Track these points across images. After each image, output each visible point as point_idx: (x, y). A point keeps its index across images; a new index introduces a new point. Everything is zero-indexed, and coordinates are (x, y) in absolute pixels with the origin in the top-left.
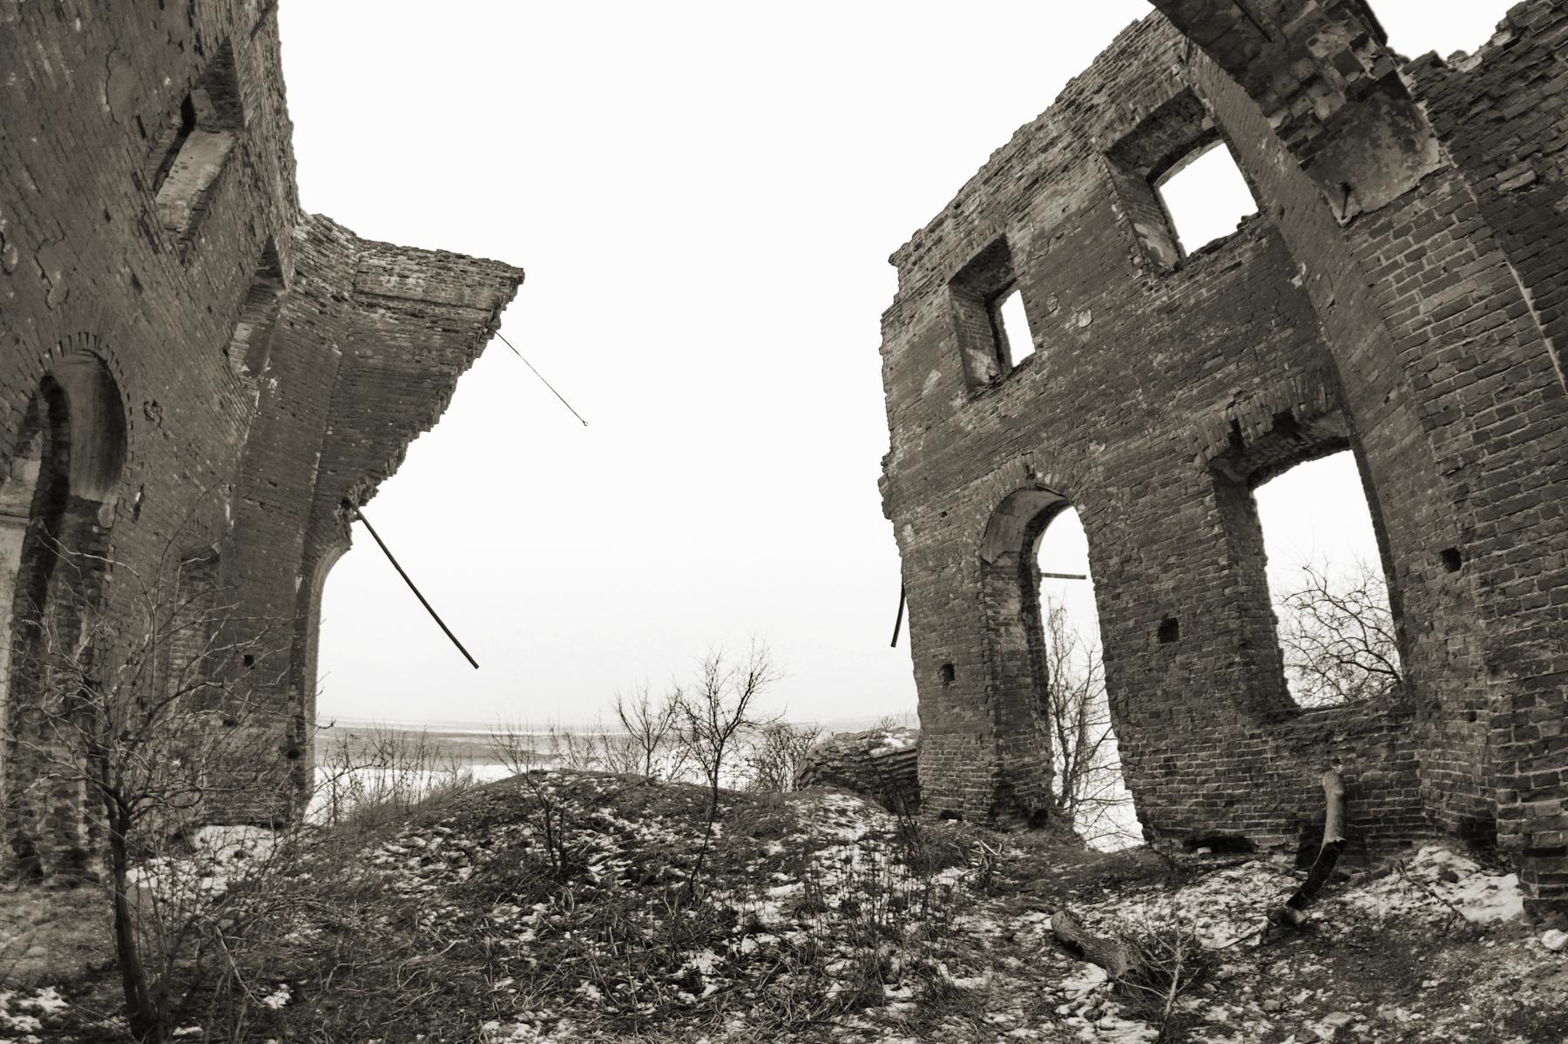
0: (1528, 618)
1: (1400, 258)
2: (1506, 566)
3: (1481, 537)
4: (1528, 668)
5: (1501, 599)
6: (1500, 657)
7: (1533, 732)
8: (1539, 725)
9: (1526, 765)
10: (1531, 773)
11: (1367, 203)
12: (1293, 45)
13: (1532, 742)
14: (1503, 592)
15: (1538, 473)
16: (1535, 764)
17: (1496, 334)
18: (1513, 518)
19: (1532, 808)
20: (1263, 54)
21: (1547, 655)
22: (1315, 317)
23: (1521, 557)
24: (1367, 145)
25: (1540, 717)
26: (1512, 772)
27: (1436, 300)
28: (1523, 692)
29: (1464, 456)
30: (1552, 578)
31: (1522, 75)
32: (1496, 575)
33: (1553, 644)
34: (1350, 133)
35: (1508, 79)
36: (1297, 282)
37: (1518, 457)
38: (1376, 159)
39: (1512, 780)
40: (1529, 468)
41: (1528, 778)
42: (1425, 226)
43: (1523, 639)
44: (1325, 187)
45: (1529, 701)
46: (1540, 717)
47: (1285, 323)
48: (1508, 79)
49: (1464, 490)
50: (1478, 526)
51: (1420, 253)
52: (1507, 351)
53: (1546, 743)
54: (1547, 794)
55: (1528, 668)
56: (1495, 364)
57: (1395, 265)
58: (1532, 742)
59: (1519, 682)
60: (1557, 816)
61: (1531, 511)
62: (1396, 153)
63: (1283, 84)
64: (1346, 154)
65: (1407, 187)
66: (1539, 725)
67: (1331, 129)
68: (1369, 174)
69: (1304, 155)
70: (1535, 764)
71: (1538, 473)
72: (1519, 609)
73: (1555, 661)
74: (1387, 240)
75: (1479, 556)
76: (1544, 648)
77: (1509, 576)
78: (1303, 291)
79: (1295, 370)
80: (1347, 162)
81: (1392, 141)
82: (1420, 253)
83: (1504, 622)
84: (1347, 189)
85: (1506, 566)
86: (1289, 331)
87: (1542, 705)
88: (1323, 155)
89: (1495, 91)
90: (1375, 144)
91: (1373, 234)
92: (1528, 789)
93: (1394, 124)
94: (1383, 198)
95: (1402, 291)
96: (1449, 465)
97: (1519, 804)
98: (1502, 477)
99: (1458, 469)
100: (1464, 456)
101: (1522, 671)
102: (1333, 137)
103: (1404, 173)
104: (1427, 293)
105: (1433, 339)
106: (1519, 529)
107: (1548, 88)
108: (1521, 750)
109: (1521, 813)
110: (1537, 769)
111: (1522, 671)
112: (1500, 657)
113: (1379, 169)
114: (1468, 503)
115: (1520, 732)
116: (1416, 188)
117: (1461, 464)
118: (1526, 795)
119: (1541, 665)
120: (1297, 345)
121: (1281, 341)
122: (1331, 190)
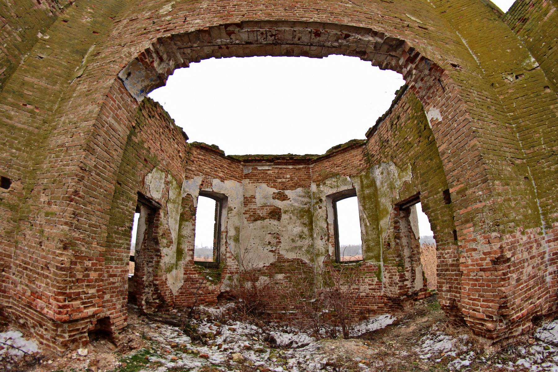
0: (82, 233)
1: (117, 102)
2: (82, 212)
3: (79, 197)
4: (78, 252)
5: (77, 223)
6: (70, 244)
7: (74, 276)
8: (77, 273)
9: (71, 288)
10: (72, 291)
11: (126, 82)
12: (173, 54)
13: (74, 279)
14: (78, 221)
15: (102, 190)
16: (73, 288)
17: (116, 147)
18: (91, 198)
19: (72, 305)
20: (175, 47)
21: (83, 249)
22: (29, 50)
23: (87, 212)
24: (143, 79)
25: (78, 271)
26: (66, 290)
27: (113, 121)
28: (74, 260)
29: (90, 168)
30: (93, 224)
31: (149, 111)
32: (79, 214)
33: (86, 246)
34: (147, 74)
35: (148, 108)
36: (40, 35)
37: (100, 182)
38: (138, 82)
39: (65, 293)
40: (101, 187)
41: (71, 293)
42: (126, 105)
43: (78, 240)
44: (129, 66)
45: (75, 264)
46: (78, 271)
47: (22, 36)
48: (148, 108)
49: (83, 178)
50: (81, 193)
51: (120, 108)
52: (114, 153)
53: (78, 280)
54: (76, 299)
55: (78, 252)
56: (111, 153)
57: (115, 101)
58: (74, 279)
59: (75, 256)
60: (79, 308)
61: (96, 200)
62: (140, 88)
63: (161, 49)
64: (140, 72)
65: (132, 94)
66: (77, 273)
67: (149, 67)
68: (134, 81)
69: (141, 58)
70: (73, 288)
71: (102, 190)
72: (80, 229)
73: (86, 252)
74: (119, 94)
75: (77, 203)
76: (84, 246)
77: (82, 217)
78: (37, 40)
79: (5, 50)
80: (137, 73)
81: (143, 86)
82: (120, 108)
83: (75, 231)
84: (129, 74)
85: (82, 212)
86: (20, 40)
87: (79, 267)
88: (140, 65)
89: (146, 105)
90: (143, 81)
91: (119, 89)
92: (71, 297)
93: (148, 85)
94: (128, 87)
95: (111, 109)
96: (84, 166)
97: (67, 303)
98: (94, 184)
99: (85, 170)
100: (90, 168)
101: (76, 252)
102: (146, 68)
103: (135, 92)
104: (113, 118)
105: (105, 129)
106: (90, 203)
107: (149, 119)
108: (70, 281)
109: (67, 306)
110: (74, 289)
111: (76, 252)
112: (70, 244)
113: (135, 84)
114: (81, 183)
115: (71, 274)
116: (132, 97)
117: (87, 169)
118: (70, 299)
119: (82, 252)
120: (16, 46)
121: (14, 37)
122: (128, 69)
